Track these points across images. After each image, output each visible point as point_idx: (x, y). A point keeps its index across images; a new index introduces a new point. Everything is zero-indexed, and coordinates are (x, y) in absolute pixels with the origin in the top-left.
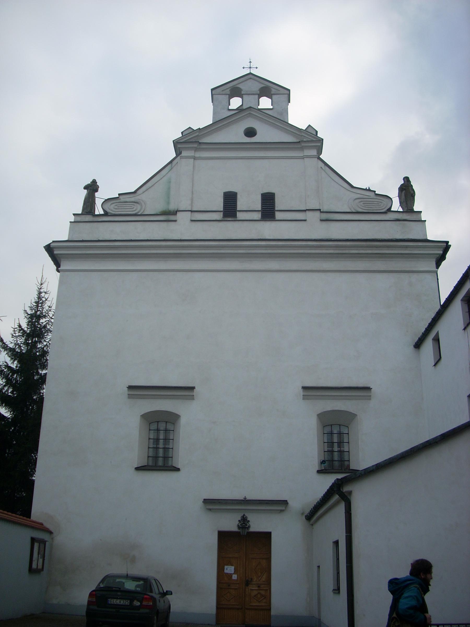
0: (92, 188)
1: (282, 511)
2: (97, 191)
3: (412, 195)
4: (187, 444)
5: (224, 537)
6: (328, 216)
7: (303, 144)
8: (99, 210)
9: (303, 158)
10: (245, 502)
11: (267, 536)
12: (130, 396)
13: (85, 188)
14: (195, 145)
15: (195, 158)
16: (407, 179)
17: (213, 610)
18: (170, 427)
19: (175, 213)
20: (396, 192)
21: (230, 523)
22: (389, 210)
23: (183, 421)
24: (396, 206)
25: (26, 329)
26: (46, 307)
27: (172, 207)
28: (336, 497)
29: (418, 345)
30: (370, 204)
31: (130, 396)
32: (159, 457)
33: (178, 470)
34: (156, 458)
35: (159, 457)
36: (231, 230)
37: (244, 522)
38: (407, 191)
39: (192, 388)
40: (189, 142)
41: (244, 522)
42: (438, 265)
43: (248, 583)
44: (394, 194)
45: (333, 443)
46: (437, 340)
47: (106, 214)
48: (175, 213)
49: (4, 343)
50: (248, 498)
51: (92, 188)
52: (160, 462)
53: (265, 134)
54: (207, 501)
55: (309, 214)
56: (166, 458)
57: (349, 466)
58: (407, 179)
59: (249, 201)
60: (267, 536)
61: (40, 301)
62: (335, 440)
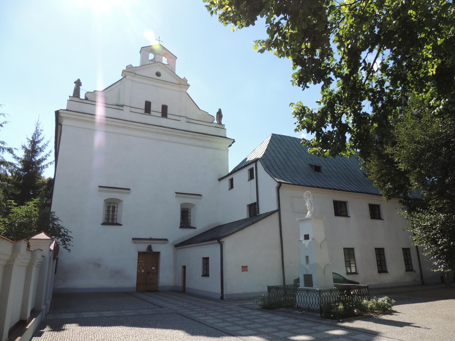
0: (78, 83)
1: (165, 243)
2: (81, 85)
3: (222, 117)
4: (124, 214)
5: (140, 253)
6: (189, 121)
7: (181, 86)
8: (82, 96)
9: (181, 92)
10: (151, 239)
11: (158, 253)
12: (99, 191)
13: (75, 83)
14: (134, 75)
15: (133, 81)
16: (220, 110)
17: (135, 286)
18: (116, 205)
19: (123, 106)
20: (216, 115)
21: (143, 248)
22: (212, 122)
23: (124, 203)
24: (215, 122)
25: (28, 148)
26: (41, 137)
27: (121, 103)
28: (216, 241)
29: (220, 180)
30: (205, 119)
31: (99, 191)
32: (111, 218)
33: (121, 225)
34: (108, 219)
35: (111, 218)
36: (147, 119)
37: (150, 248)
38: (220, 114)
39: (129, 189)
40: (129, 71)
41: (150, 248)
42: (229, 146)
43: (148, 273)
44: (215, 115)
45: (109, 219)
46: (232, 180)
47: (86, 99)
48: (123, 106)
49: (14, 155)
50: (152, 238)
51: (78, 83)
52: (110, 221)
53: (165, 76)
54: (134, 239)
55: (182, 119)
56: (113, 219)
57: (190, 225)
58: (220, 110)
59: (156, 107)
60: (158, 253)
61: (37, 134)
62: (111, 217)
